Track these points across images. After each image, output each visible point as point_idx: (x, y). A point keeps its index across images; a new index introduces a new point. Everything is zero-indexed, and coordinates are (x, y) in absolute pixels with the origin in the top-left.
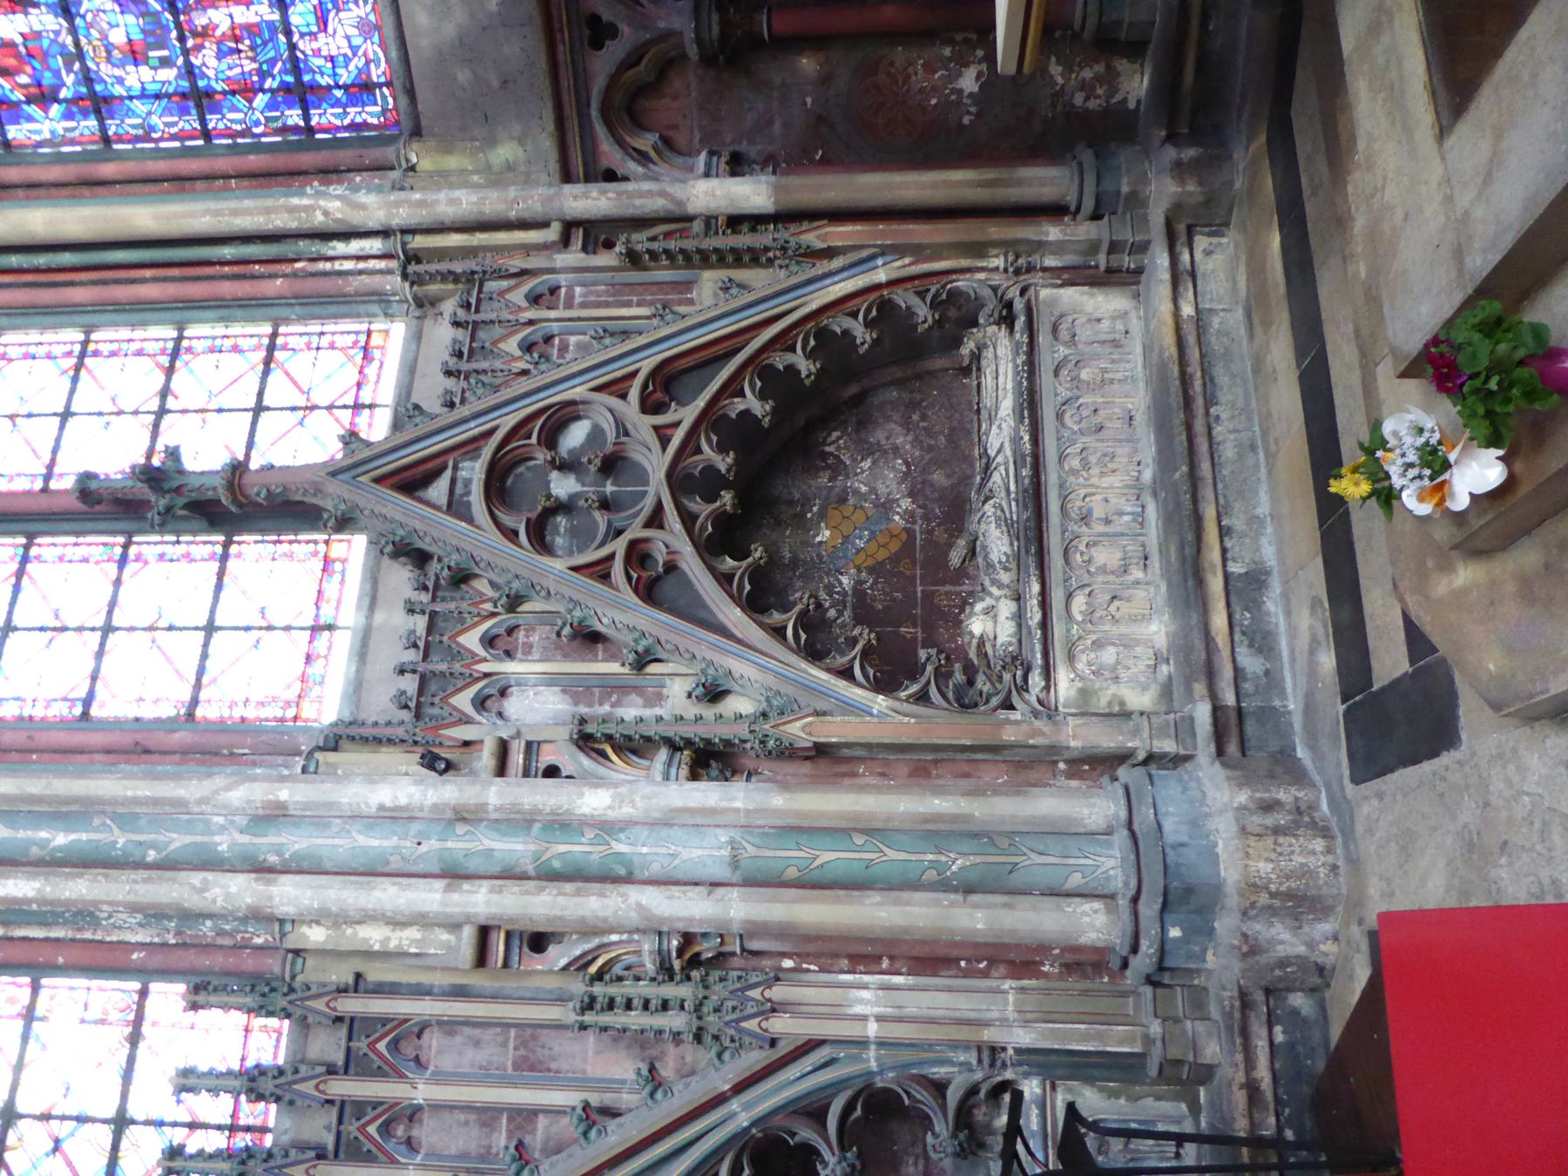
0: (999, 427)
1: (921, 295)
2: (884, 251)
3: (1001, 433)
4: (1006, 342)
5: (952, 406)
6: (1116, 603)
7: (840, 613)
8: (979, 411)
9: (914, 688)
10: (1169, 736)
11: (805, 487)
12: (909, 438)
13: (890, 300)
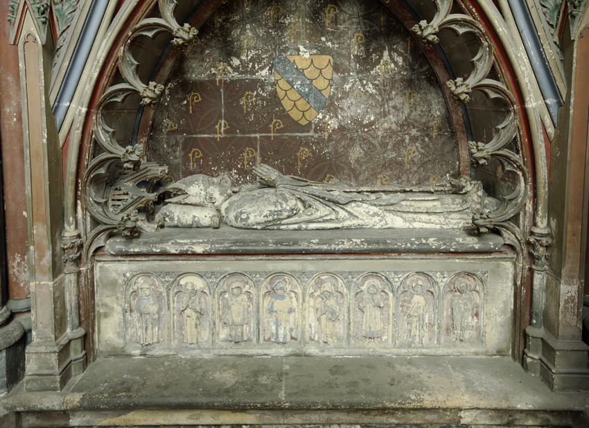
0: (375, 214)
1: (512, 145)
2: (563, 105)
3: (368, 215)
6: (194, 315)
7: (236, 69)
9: (104, 138)
10: (40, 368)
11: (350, 33)
12: (394, 126)
13: (509, 112)
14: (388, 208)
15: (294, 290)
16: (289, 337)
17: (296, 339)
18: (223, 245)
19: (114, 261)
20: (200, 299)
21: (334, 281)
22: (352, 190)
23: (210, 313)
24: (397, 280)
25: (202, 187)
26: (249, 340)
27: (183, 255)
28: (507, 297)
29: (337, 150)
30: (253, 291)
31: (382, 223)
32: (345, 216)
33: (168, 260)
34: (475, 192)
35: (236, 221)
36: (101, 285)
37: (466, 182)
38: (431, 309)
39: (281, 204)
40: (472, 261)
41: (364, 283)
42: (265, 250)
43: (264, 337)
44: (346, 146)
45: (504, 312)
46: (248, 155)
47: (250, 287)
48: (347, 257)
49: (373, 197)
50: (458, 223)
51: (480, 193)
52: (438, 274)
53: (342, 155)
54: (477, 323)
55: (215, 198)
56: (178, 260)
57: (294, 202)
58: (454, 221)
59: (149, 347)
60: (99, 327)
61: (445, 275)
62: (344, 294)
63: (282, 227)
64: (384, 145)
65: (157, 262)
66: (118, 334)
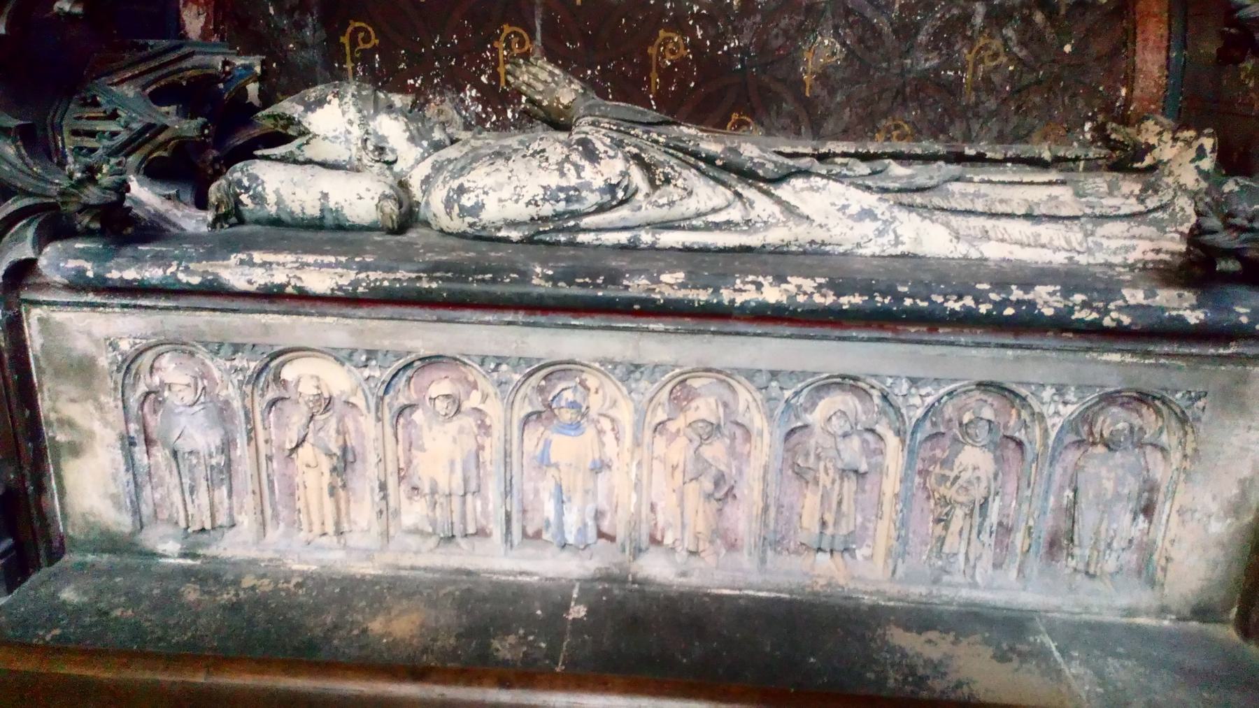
3: (840, 212)
14: (906, 198)
16: (592, 532)
17: (612, 539)
18: (392, 276)
19: (77, 304)
21: (727, 395)
22: (801, 150)
25: (352, 113)
26: (482, 533)
27: (271, 296)
31: (884, 240)
33: (234, 311)
35: (449, 214)
36: (49, 371)
37: (1160, 133)
38: (1011, 487)
39: (579, 169)
40: (1162, 361)
42: (520, 295)
47: (485, 397)
48: (769, 328)
49: (863, 168)
50: (1127, 249)
51: (1207, 164)
52: (1048, 393)
53: (781, 58)
55: (393, 151)
56: (266, 312)
57: (619, 165)
58: (1114, 244)
61: (1071, 397)
62: (754, 432)
63: (581, 238)
64: (905, 31)
66: (115, 499)
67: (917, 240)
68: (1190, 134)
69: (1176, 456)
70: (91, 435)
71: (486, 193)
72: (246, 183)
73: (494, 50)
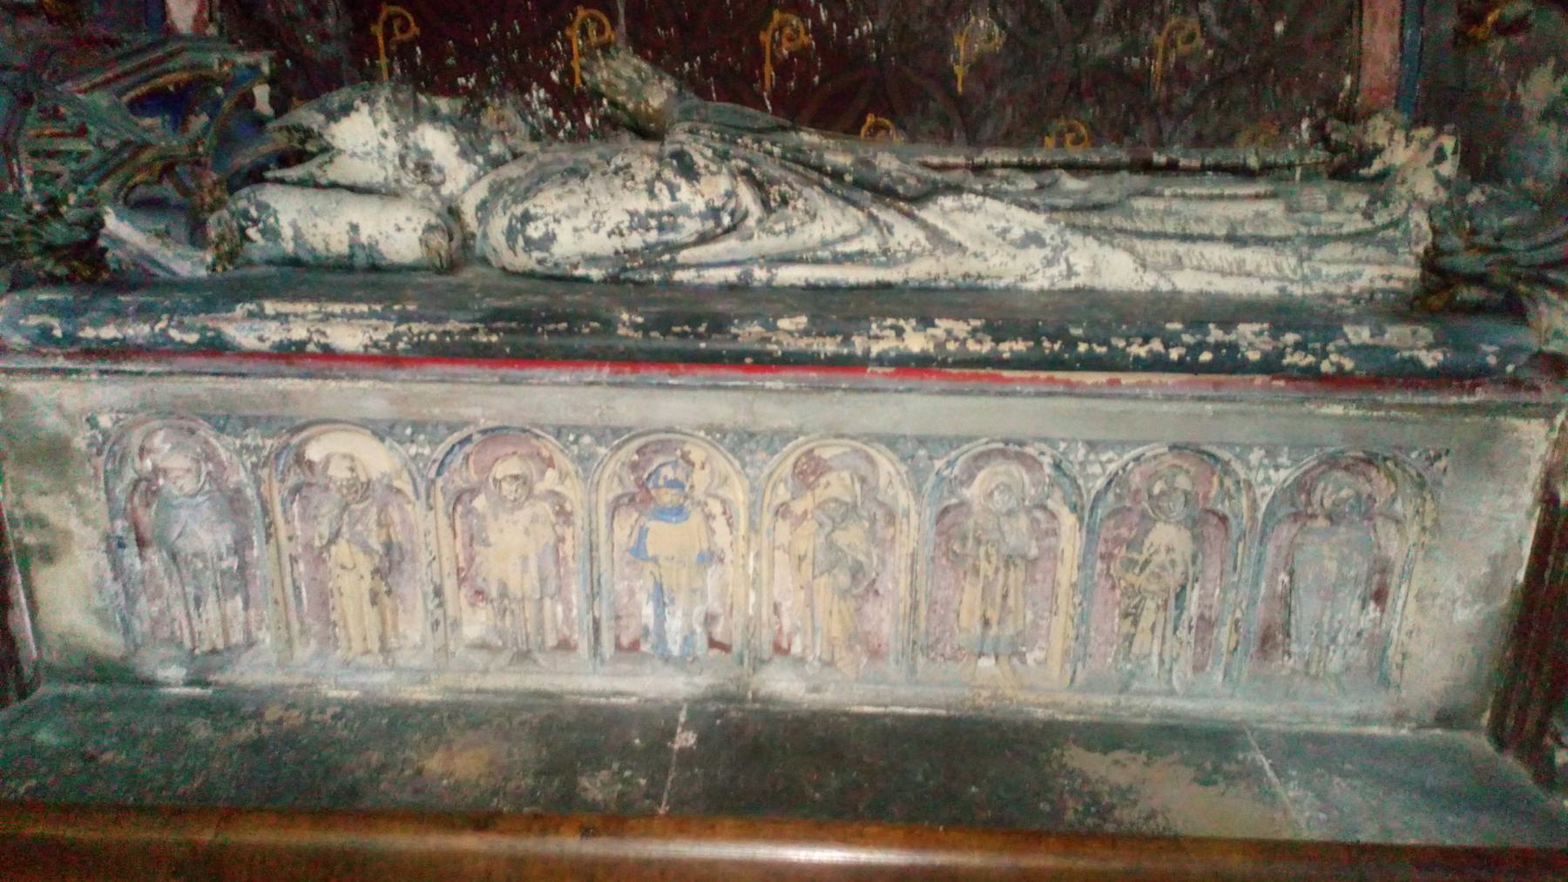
0: (1033, 239)
4: (1370, 276)
5: (1222, 82)
8: (1147, 167)
14: (1079, 219)
15: (721, 492)
16: (701, 642)
17: (725, 648)
20: (382, 509)
22: (951, 160)
23: (424, 557)
24: (1097, 469)
25: (386, 123)
26: (565, 645)
27: (289, 355)
28: (1506, 541)
29: (905, 27)
30: (573, 493)
32: (917, 242)
34: (1430, 165)
35: (512, 248)
37: (1391, 132)
39: (673, 190)
41: (972, 477)
43: (617, 638)
44: (940, 13)
45: (1486, 592)
46: (584, 33)
47: (563, 476)
50: (1351, 277)
51: (1448, 169)
54: (1377, 623)
55: (440, 170)
58: (1334, 270)
59: (216, 659)
60: (30, 596)
61: (1283, 460)
63: (679, 276)
65: (207, 382)
67: (1095, 270)
68: (1425, 132)
69: (1413, 530)
70: (67, 535)
71: (557, 221)
72: (254, 213)
73: (567, 41)
